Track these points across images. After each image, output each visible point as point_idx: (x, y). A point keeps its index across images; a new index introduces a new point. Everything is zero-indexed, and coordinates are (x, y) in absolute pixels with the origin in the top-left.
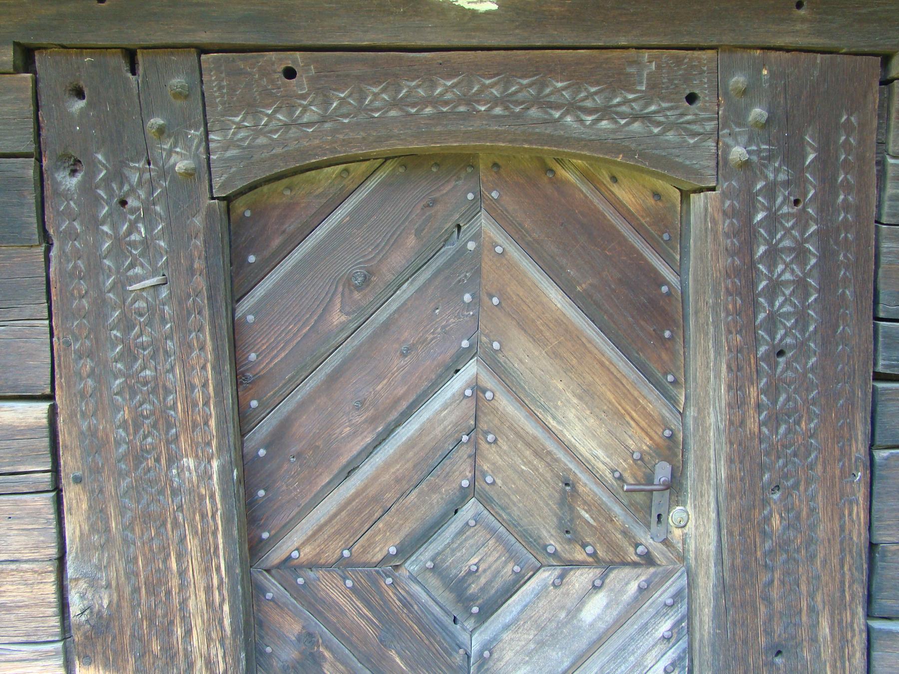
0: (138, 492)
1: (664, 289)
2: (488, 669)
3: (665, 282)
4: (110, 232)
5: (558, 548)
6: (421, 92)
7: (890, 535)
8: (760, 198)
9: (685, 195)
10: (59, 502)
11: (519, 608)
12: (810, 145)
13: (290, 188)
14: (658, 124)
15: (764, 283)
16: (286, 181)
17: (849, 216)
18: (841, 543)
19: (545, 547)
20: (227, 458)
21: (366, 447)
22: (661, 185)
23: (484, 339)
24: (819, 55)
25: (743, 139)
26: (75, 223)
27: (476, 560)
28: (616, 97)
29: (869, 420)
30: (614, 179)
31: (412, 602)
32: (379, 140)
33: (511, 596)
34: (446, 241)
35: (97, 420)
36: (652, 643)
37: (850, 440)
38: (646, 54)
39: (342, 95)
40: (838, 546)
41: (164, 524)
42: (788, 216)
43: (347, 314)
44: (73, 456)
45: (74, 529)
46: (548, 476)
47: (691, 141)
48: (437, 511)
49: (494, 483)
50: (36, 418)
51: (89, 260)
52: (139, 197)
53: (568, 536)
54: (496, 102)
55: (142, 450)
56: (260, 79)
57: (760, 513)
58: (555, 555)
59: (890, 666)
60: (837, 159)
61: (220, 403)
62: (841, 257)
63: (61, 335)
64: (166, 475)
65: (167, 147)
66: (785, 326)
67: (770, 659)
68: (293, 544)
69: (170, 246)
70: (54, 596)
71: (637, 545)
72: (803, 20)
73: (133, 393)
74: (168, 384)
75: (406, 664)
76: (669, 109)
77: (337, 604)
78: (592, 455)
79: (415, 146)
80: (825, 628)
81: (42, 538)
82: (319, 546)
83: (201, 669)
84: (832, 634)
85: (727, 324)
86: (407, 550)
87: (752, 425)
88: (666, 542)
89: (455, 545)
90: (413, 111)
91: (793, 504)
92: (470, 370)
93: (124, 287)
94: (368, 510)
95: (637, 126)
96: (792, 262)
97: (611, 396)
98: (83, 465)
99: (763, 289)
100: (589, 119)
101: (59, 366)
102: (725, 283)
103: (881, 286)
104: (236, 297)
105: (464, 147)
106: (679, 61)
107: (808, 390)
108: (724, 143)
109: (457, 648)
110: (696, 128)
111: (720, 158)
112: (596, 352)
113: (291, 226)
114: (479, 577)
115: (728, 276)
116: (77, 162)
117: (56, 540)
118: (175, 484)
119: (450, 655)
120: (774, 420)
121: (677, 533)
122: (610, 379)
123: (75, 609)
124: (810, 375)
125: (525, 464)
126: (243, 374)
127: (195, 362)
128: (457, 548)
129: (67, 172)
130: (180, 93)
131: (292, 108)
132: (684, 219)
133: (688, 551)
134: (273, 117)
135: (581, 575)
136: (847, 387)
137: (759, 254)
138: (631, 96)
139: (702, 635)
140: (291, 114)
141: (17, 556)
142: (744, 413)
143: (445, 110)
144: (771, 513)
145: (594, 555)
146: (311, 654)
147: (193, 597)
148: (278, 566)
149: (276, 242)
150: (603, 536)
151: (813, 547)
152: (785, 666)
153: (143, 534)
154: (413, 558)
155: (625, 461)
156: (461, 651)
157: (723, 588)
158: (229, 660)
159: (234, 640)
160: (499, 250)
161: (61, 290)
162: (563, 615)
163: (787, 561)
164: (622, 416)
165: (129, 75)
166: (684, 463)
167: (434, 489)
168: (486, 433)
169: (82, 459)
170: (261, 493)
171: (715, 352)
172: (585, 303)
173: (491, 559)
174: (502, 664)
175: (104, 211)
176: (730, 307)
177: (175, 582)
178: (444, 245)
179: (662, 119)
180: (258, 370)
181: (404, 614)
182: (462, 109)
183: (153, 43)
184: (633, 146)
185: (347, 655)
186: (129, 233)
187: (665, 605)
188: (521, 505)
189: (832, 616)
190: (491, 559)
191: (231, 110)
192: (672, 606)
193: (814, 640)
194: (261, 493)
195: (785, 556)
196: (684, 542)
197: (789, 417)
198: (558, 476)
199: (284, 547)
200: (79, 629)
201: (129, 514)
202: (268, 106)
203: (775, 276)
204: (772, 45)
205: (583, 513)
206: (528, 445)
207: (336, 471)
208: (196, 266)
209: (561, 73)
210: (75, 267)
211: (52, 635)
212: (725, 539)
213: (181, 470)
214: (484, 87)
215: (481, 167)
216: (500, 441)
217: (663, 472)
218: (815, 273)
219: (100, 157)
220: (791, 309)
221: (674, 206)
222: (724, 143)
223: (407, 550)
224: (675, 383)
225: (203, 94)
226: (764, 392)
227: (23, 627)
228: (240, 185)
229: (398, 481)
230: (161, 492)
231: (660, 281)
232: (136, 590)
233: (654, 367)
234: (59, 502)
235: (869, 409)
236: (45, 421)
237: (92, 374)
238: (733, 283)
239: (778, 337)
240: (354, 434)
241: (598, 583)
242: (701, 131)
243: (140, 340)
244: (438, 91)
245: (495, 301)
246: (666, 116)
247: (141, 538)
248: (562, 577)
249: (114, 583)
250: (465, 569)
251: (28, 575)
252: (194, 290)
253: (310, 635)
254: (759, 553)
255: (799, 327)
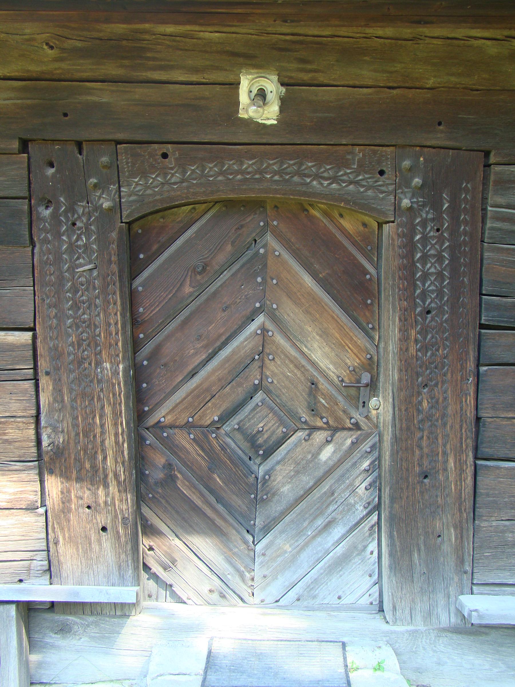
0: (79, 381)
1: (368, 277)
2: (268, 486)
3: (369, 273)
4: (67, 240)
5: (307, 419)
6: (235, 167)
7: (488, 413)
8: (418, 227)
9: (380, 225)
10: (37, 386)
11: (285, 452)
12: (446, 199)
13: (163, 217)
14: (363, 186)
15: (420, 273)
16: (161, 214)
17: (466, 238)
18: (461, 416)
19: (300, 418)
20: (127, 364)
21: (202, 361)
22: (366, 219)
23: (268, 302)
24: (451, 151)
25: (409, 195)
26: (48, 235)
27: (262, 425)
28: (340, 171)
29: (476, 349)
30: (341, 216)
31: (226, 447)
32: (212, 193)
33: (281, 446)
34: (248, 248)
35: (58, 341)
36: (359, 473)
37: (466, 360)
38: (357, 148)
39: (193, 168)
40: (459, 419)
41: (93, 399)
42: (433, 237)
43: (193, 287)
44: (45, 360)
45: (45, 400)
46: (303, 379)
47: (381, 196)
48: (241, 397)
49: (272, 382)
50: (26, 340)
51: (55, 254)
52: (83, 221)
53: (313, 412)
54: (275, 173)
55: (82, 358)
56: (149, 158)
57: (416, 400)
58: (306, 422)
59: (487, 485)
60: (460, 207)
61: (124, 333)
62: (462, 260)
63: (40, 295)
64: (95, 372)
65: (98, 194)
66: (431, 297)
67: (421, 479)
68: (162, 414)
69: (99, 248)
70: (34, 436)
71: (351, 418)
72: (442, 132)
73: (78, 327)
74: (97, 323)
75: (223, 482)
76: (369, 178)
77: (185, 448)
78: (327, 368)
79: (232, 196)
80: (451, 463)
81: (28, 405)
82: (176, 415)
83: (112, 478)
84: (455, 466)
85: (399, 295)
86: (225, 418)
87: (412, 350)
88: (367, 417)
89: (250, 416)
90: (231, 177)
91: (434, 395)
92: (260, 319)
93: (74, 269)
94: (204, 396)
95: (351, 187)
96: (435, 262)
97: (337, 335)
98: (50, 365)
99: (419, 277)
100: (326, 183)
101: (39, 311)
102: (398, 273)
103: (484, 276)
104: (133, 277)
105: (258, 197)
106: (375, 152)
107: (444, 332)
108: (399, 197)
109: (251, 474)
110: (384, 189)
111: (396, 206)
112: (330, 311)
113: (163, 238)
114: (263, 434)
115: (400, 269)
116: (50, 202)
117: (35, 406)
118: (99, 377)
119: (247, 477)
120: (425, 348)
121: (374, 412)
122: (337, 326)
123: (45, 443)
124: (445, 325)
125: (290, 372)
126: (136, 319)
127: (111, 311)
128: (251, 418)
129: (44, 207)
130: (106, 166)
131: (165, 175)
132: (380, 238)
133: (380, 423)
134: (155, 179)
135: (320, 434)
136: (465, 331)
137: (417, 258)
138: (348, 171)
139: (385, 468)
140: (165, 177)
141: (15, 414)
142: (408, 344)
143: (248, 177)
144: (422, 399)
145: (327, 423)
146: (171, 475)
147: (108, 439)
148: (153, 426)
149: (155, 247)
150: (333, 413)
151: (446, 418)
152: (429, 483)
153: (81, 404)
154: (227, 423)
155: (345, 371)
156: (253, 476)
157: (396, 440)
158: (127, 473)
159: (130, 463)
160: (277, 253)
161: (40, 271)
162: (309, 456)
163: (431, 426)
164: (344, 346)
165: (79, 155)
166: (378, 374)
167: (240, 385)
168: (269, 354)
169: (50, 362)
170: (145, 385)
171: (392, 310)
172: (324, 284)
173: (270, 425)
174: (276, 483)
175: (64, 229)
176: (401, 286)
177: (98, 430)
178: (247, 251)
179: (365, 184)
180: (144, 317)
181: (222, 455)
182: (257, 176)
183: (93, 139)
184: (349, 198)
185: (190, 477)
186: (77, 240)
187: (366, 452)
188: (287, 395)
189: (455, 456)
190: (270, 425)
191: (133, 175)
192: (370, 452)
193: (445, 470)
194: (145, 385)
195: (430, 423)
196: (378, 418)
197: (433, 347)
198: (308, 379)
199: (156, 416)
200: (47, 454)
201: (74, 393)
202: (153, 173)
203: (426, 270)
204: (425, 145)
205: (321, 400)
206: (292, 362)
207: (185, 374)
208: (113, 259)
209: (311, 158)
210: (48, 258)
211: (33, 457)
212: (397, 413)
213: (103, 369)
214: (269, 165)
215: (268, 208)
216: (276, 359)
217: (366, 378)
218: (448, 269)
219: (62, 199)
220: (434, 288)
221: (374, 231)
222: (399, 197)
223: (225, 418)
224: (373, 329)
225: (118, 166)
226: (419, 333)
227: (18, 452)
228: (136, 216)
229: (220, 380)
230: (91, 381)
231: (365, 272)
232: (78, 434)
233: (361, 319)
234: (37, 386)
235: (477, 343)
236: (30, 341)
237: (56, 316)
238: (403, 273)
239: (427, 303)
240: (196, 354)
241: (329, 439)
242: (387, 190)
243: (82, 298)
244: (244, 167)
245: (275, 281)
246: (368, 182)
247: (81, 406)
248: (309, 435)
249: (66, 430)
250: (256, 430)
251: (20, 424)
252: (111, 272)
253: (170, 465)
254: (415, 421)
255: (439, 298)
